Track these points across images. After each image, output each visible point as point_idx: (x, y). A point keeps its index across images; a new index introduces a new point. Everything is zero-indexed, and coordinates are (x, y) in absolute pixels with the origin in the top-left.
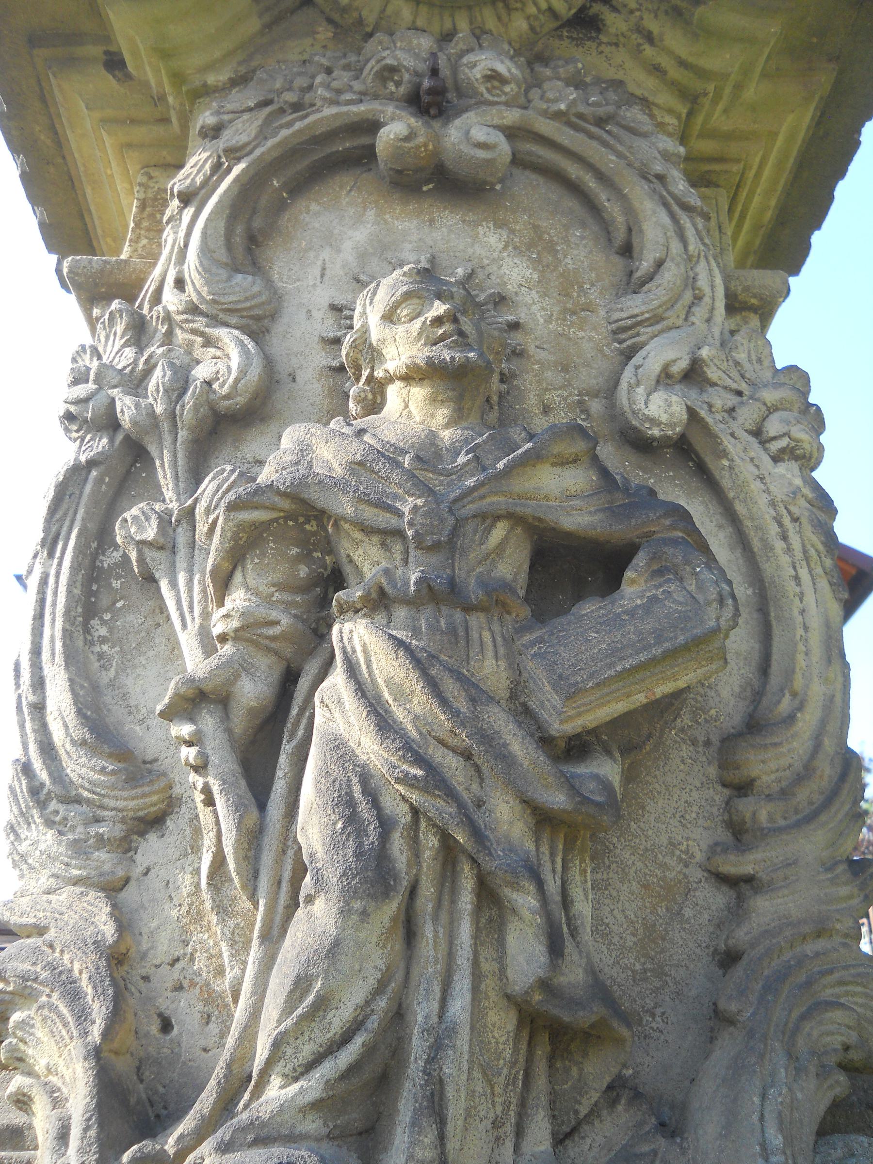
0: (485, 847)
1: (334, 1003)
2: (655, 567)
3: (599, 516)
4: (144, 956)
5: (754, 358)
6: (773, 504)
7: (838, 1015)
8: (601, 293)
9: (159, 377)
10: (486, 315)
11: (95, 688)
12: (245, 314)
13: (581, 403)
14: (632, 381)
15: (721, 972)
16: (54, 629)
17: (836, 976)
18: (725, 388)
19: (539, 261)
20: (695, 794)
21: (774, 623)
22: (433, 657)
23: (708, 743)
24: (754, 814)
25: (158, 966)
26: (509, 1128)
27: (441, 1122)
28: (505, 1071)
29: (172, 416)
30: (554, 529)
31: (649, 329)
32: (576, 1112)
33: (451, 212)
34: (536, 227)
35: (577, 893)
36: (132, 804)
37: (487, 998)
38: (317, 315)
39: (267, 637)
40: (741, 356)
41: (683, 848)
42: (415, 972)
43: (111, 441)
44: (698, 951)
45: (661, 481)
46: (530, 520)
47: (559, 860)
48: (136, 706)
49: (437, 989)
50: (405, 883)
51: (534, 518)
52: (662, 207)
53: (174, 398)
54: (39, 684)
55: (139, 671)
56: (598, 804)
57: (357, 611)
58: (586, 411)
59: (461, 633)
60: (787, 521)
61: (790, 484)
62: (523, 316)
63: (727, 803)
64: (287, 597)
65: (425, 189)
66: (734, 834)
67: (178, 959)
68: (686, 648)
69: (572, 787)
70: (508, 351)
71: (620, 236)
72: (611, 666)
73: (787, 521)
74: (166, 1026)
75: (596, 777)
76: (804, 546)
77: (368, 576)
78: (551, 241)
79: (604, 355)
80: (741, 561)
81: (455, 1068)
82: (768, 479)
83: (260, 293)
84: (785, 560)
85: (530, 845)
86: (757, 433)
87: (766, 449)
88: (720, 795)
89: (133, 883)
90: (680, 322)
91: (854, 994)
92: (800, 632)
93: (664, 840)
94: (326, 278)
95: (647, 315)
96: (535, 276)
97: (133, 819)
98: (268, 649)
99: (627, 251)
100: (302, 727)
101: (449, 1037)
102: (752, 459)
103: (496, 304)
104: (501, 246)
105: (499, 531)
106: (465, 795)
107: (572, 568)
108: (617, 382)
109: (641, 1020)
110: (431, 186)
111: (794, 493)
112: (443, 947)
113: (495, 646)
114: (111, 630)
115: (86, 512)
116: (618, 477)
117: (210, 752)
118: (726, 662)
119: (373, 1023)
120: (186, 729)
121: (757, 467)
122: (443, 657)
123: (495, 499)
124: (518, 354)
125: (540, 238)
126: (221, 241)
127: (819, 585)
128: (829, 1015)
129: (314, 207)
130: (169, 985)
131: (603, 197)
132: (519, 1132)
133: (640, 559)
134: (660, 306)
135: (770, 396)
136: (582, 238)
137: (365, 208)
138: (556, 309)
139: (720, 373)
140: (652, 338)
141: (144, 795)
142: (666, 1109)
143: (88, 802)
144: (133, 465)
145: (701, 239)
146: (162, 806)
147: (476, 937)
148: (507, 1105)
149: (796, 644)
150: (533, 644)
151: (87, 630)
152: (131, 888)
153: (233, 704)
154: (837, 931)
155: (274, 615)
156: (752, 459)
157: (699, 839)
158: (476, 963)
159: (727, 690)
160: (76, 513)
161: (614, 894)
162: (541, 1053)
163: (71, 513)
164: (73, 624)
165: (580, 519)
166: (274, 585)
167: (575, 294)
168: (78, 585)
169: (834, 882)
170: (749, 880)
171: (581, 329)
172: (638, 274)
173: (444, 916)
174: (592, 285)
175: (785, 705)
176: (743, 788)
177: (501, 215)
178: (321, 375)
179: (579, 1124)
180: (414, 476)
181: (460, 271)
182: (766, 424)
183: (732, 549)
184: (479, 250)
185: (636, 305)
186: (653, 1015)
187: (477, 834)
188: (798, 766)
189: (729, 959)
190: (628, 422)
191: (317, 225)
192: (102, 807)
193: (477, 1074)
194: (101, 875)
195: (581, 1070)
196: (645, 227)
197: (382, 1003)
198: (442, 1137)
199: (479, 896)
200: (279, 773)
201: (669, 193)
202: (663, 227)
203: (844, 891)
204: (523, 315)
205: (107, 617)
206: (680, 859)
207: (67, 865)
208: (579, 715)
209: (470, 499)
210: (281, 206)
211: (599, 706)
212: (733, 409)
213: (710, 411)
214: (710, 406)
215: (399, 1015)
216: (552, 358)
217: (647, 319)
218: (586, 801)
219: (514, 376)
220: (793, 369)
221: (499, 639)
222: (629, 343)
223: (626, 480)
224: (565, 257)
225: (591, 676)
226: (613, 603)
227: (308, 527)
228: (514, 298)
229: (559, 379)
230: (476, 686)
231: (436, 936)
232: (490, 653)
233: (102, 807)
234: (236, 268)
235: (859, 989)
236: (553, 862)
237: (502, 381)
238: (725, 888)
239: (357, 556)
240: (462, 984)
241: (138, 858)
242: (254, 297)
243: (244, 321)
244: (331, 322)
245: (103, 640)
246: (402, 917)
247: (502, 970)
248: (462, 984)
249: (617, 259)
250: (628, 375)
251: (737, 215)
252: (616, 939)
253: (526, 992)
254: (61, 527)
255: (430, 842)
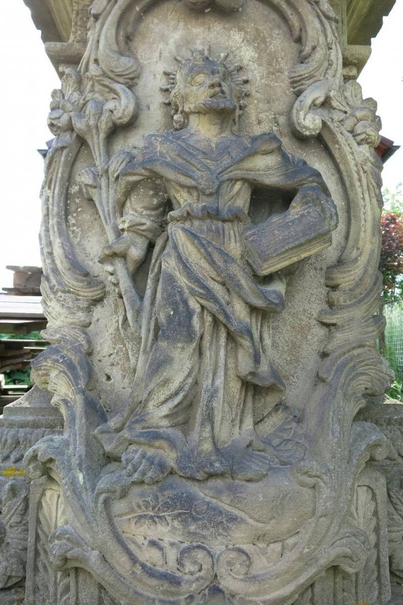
0: (230, 322)
1: (172, 381)
2: (304, 200)
3: (281, 177)
4: (99, 352)
5: (354, 95)
6: (356, 165)
7: (364, 377)
8: (286, 63)
9: (90, 108)
10: (233, 77)
11: (72, 246)
12: (126, 77)
13: (275, 118)
14: (299, 109)
15: (320, 360)
16: (53, 221)
17: (365, 363)
18: (340, 110)
19: (258, 47)
20: (315, 290)
21: (352, 218)
22: (209, 242)
23: (321, 269)
24: (338, 298)
25: (104, 357)
26: (237, 421)
27: (212, 424)
28: (236, 403)
29: (97, 127)
30: (261, 184)
31: (307, 82)
32: (263, 414)
33: (218, 23)
34: (257, 30)
35: (266, 336)
36: (90, 294)
37: (230, 377)
38: (159, 77)
39: (141, 230)
40: (348, 94)
41: (309, 312)
42: (202, 368)
43: (71, 137)
44: (312, 352)
45: (308, 154)
46: (251, 181)
47: (259, 324)
48: (89, 253)
49: (211, 375)
50: (198, 335)
51: (253, 179)
52: (317, 19)
53: (97, 118)
54: (50, 244)
55: (89, 238)
56: (276, 304)
57: (178, 221)
58: (277, 122)
59: (221, 232)
60: (361, 173)
61: (364, 156)
62: (249, 76)
63: (328, 294)
64: (149, 212)
65: (206, 11)
66: (330, 306)
67: (112, 354)
68: (315, 238)
69: (266, 298)
70: (243, 95)
71: (296, 33)
72: (283, 247)
73: (361, 173)
74: (109, 378)
75: (274, 292)
76: (368, 184)
77: (183, 206)
78: (264, 37)
79: (286, 95)
80: (340, 190)
81: (218, 405)
82: (355, 153)
83: (132, 66)
84: (359, 190)
85: (248, 320)
86: (351, 132)
87: (355, 139)
88: (324, 291)
89: (92, 324)
90: (322, 78)
91: (371, 369)
92: (363, 222)
93: (301, 309)
94: (162, 58)
95: (306, 75)
96: (256, 55)
97: (91, 300)
98: (142, 235)
99: (299, 40)
100: (156, 267)
101: (216, 393)
102: (349, 145)
103: (238, 71)
104: (241, 40)
105: (238, 186)
106: (223, 301)
107: (268, 199)
108: (292, 108)
109: (289, 378)
110: (209, 10)
111: (366, 160)
112: (213, 358)
113: (235, 237)
114: (76, 220)
115: (63, 170)
116: (290, 156)
117: (120, 278)
118: (331, 243)
119: (187, 387)
120: (110, 268)
121: (351, 148)
122: (214, 242)
123: (236, 172)
124: (247, 95)
125: (259, 36)
126: (114, 40)
127: (372, 201)
128: (360, 378)
129: (156, 21)
130: (109, 364)
131: (289, 12)
132: (241, 422)
133: (298, 198)
134: (313, 70)
135: (359, 114)
136: (278, 34)
137: (179, 22)
138: (265, 72)
139: (338, 103)
140: (308, 86)
141: (94, 291)
142: (297, 411)
143: (73, 293)
144: (81, 147)
145: (334, 34)
146: (102, 295)
147: (226, 355)
148: (236, 415)
149: (361, 228)
150: (251, 235)
151: (67, 221)
152: (92, 326)
153: (128, 258)
154: (367, 345)
155: (144, 221)
156: (349, 145)
157: (316, 308)
158: (226, 364)
159: (331, 253)
160: (58, 170)
161: (281, 331)
162: (250, 394)
163: (56, 170)
164: (61, 219)
165: (273, 179)
166: (143, 208)
167: (274, 64)
168: (62, 202)
169: (367, 326)
170: (334, 325)
171: (276, 82)
172: (304, 53)
173: (214, 348)
174: (282, 59)
175: (355, 253)
176: (334, 288)
177: (241, 24)
178: (161, 106)
179: (264, 418)
180: (202, 162)
181: (222, 55)
182: (356, 127)
183: (337, 185)
184: (231, 43)
185: (303, 70)
186: (293, 377)
187: (227, 316)
188: (357, 279)
189: (324, 355)
190: (295, 127)
191: (157, 30)
192: (78, 295)
193: (226, 405)
194: (81, 322)
195: (265, 400)
196: (308, 29)
197: (190, 380)
198: (212, 428)
199: (227, 339)
200: (148, 287)
201: (320, 10)
202: (317, 30)
203: (370, 329)
204: (250, 76)
205: (75, 215)
206: (307, 317)
207: (66, 317)
208: (269, 267)
209: (226, 172)
210: (139, 20)
211: (277, 264)
212: (342, 120)
213: (332, 122)
214: (332, 119)
215: (196, 383)
216: (263, 97)
217: (307, 77)
218: (271, 303)
219: (246, 106)
220: (370, 100)
221: (237, 234)
222: (297, 89)
223: (293, 157)
224: (270, 45)
225: (275, 251)
226: (285, 217)
227: (157, 182)
228: (246, 67)
229: (266, 107)
230: (227, 255)
231: (211, 355)
232: (233, 240)
233: (78, 295)
234: (121, 54)
235: (373, 367)
236: (257, 325)
237: (240, 109)
238: (324, 327)
239: (178, 196)
240: (221, 373)
241: (94, 314)
242: (130, 68)
243: (126, 80)
244: (164, 80)
245: (74, 225)
246: (198, 348)
247: (236, 366)
248: (221, 373)
249: (293, 44)
250: (297, 103)
251: (350, 12)
252: (281, 348)
253: (245, 376)
254: (53, 175)
255: (209, 319)
